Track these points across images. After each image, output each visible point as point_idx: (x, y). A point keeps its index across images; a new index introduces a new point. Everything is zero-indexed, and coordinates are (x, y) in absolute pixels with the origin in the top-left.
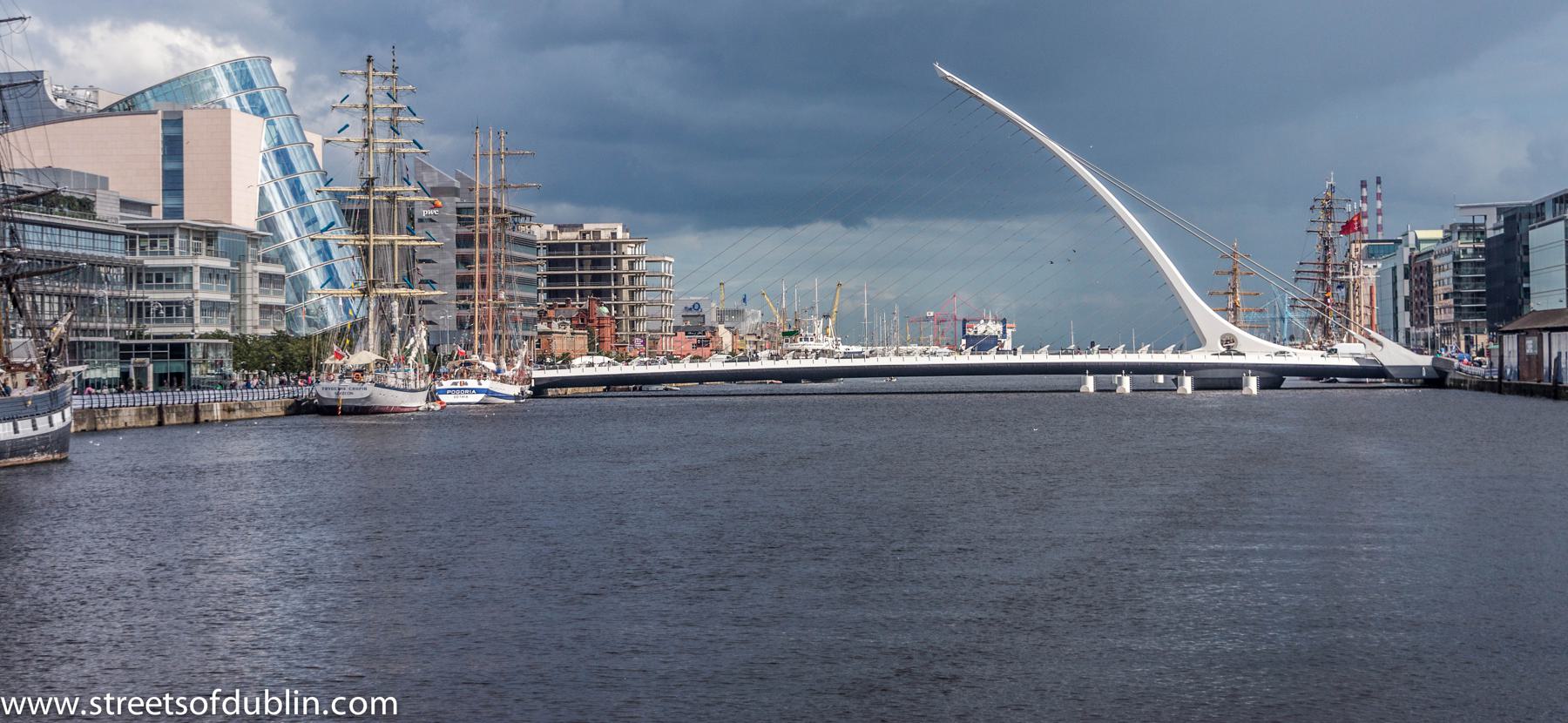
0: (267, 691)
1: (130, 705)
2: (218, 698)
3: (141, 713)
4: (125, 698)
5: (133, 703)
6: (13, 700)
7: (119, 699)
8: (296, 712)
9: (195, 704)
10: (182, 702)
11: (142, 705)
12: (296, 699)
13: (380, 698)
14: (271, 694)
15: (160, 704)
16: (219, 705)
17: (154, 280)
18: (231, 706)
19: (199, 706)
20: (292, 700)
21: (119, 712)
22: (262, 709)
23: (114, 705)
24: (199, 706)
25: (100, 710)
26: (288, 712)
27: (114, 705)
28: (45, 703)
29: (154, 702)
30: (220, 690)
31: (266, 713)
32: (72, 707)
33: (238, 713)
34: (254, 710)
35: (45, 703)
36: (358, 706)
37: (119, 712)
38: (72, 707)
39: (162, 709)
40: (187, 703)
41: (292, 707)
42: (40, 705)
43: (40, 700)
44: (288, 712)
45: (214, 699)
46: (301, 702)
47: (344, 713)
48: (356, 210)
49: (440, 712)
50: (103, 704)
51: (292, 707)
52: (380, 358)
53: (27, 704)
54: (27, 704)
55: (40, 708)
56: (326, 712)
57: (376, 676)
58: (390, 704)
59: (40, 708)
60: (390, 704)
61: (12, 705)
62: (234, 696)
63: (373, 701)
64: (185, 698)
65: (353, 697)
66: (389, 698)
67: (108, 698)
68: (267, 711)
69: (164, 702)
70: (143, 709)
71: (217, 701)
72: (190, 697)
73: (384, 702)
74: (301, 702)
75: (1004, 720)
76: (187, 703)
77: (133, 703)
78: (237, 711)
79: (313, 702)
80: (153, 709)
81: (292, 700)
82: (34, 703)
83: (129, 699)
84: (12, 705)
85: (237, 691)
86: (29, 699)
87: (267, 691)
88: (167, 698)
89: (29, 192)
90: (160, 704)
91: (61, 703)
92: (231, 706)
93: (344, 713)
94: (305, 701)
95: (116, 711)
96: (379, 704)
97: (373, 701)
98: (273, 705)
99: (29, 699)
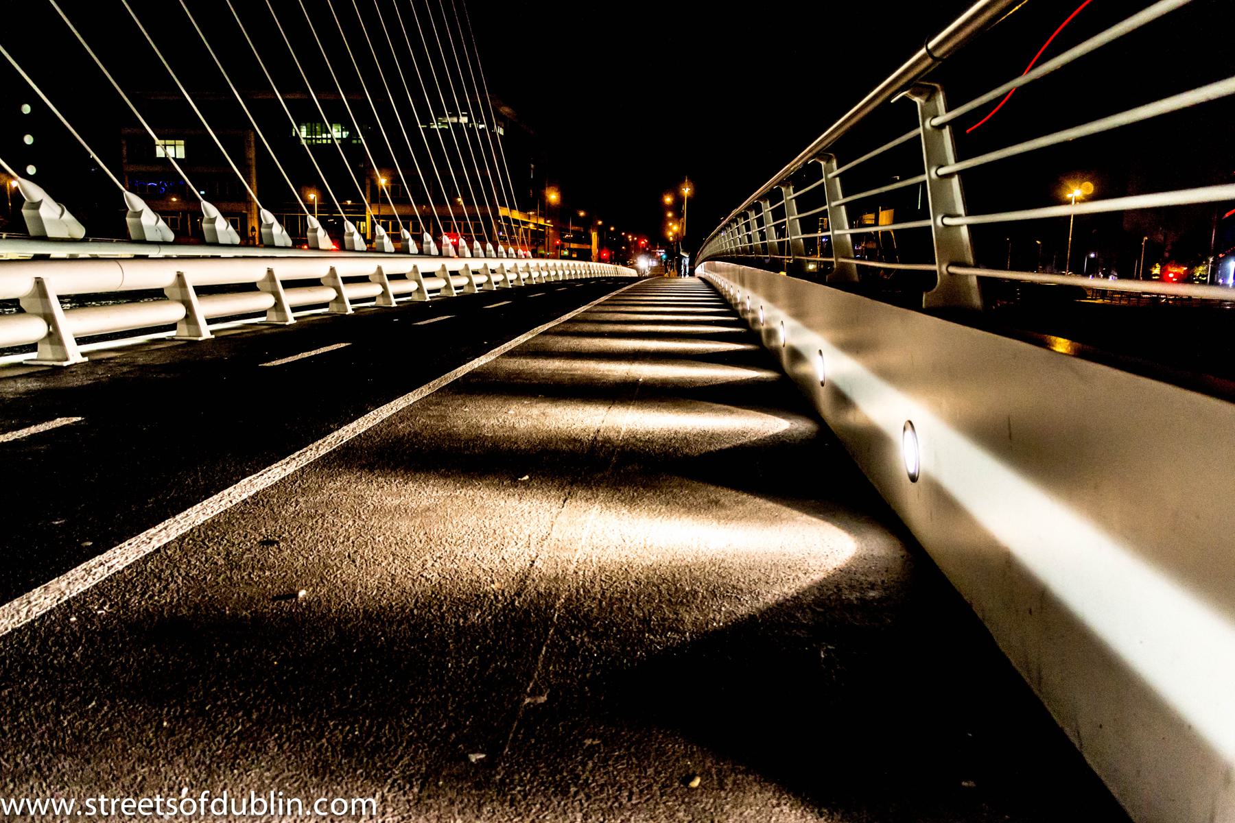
1: (123, 806)
5: (126, 804)
6: (13, 801)
12: (281, 801)
13: (370, 799)
16: (207, 804)
17: (853, 231)
20: (276, 802)
22: (249, 809)
23: (108, 805)
27: (108, 805)
29: (130, 803)
45: (203, 800)
48: (685, 275)
50: (98, 805)
51: (276, 808)
52: (622, 433)
54: (26, 806)
61: (10, 807)
63: (289, 802)
67: (102, 799)
68: (253, 811)
69: (155, 803)
75: (3, 781)
77: (126, 804)
78: (225, 811)
80: (146, 810)
81: (276, 802)
84: (10, 807)
88: (158, 799)
90: (151, 806)
91: (58, 805)
94: (289, 802)
99: (28, 800)
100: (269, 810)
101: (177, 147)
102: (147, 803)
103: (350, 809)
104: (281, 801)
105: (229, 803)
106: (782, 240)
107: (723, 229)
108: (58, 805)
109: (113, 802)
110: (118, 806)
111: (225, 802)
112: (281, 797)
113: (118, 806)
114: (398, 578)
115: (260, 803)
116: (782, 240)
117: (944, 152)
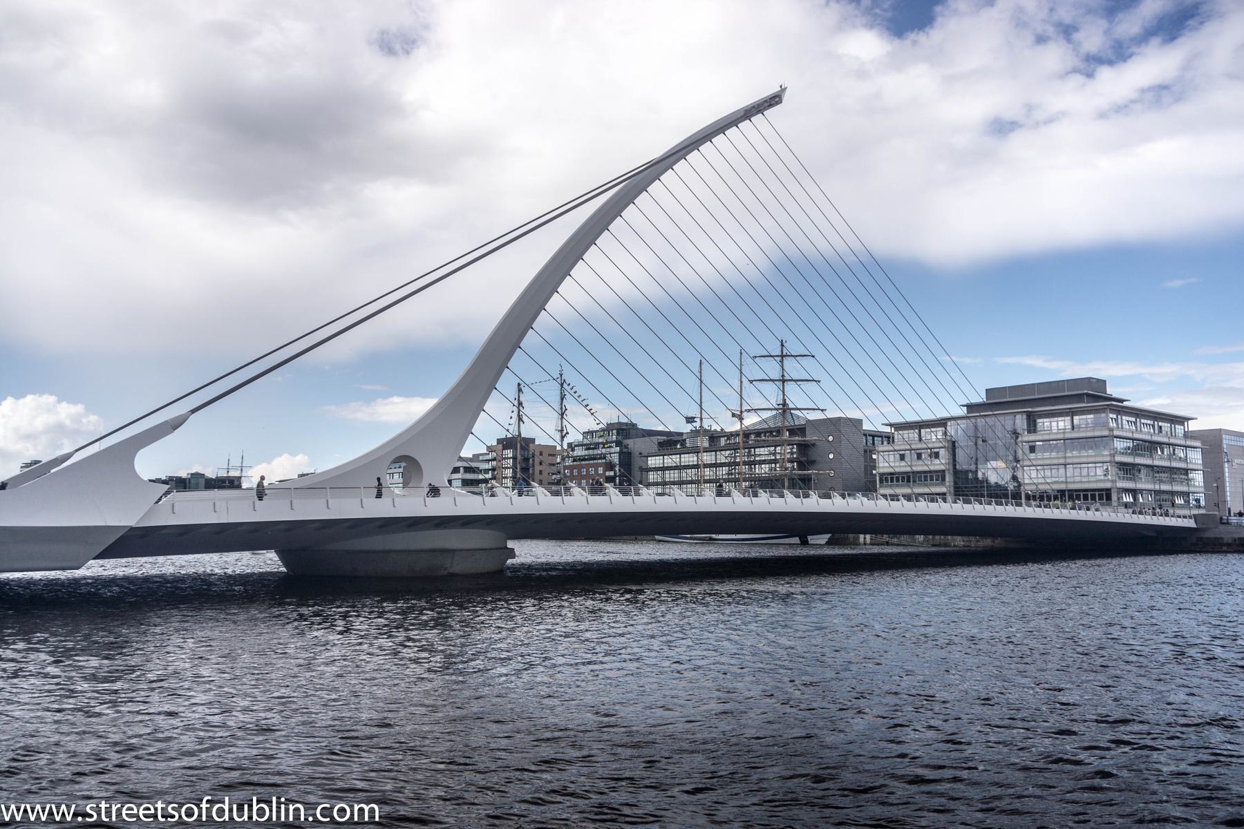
0: (255, 799)
1: (124, 812)
2: (208, 806)
3: (135, 819)
4: (119, 806)
5: (144, 809)
7: (113, 806)
8: (283, 819)
9: (217, 809)
10: (173, 809)
11: (135, 811)
14: (259, 802)
15: (152, 811)
16: (209, 810)
18: (221, 812)
19: (189, 813)
20: (279, 808)
21: (114, 819)
24: (189, 813)
25: (177, 816)
26: (274, 819)
28: (18, 810)
29: (148, 809)
30: (209, 798)
31: (254, 820)
32: (69, 814)
33: (227, 820)
34: (294, 810)
35: (18, 810)
36: (342, 811)
37: (114, 819)
38: (69, 814)
39: (155, 816)
40: (178, 810)
41: (279, 812)
42: (38, 812)
43: (63, 807)
44: (274, 819)
45: (204, 805)
46: (287, 810)
47: (328, 819)
49: (594, 620)
51: (279, 812)
53: (25, 811)
54: (25, 811)
55: (13, 815)
56: (311, 819)
57: (70, 704)
58: (372, 811)
59: (13, 815)
60: (372, 811)
62: (223, 802)
64: (176, 806)
65: (184, 804)
66: (108, 820)
67: (103, 805)
68: (255, 817)
69: (156, 809)
70: (137, 816)
71: (162, 808)
72: (181, 805)
73: (366, 808)
74: (287, 810)
76: (178, 810)
77: (144, 809)
78: (226, 817)
79: (373, 808)
80: (145, 816)
81: (279, 808)
82: (58, 808)
83: (122, 806)
85: (227, 799)
86: (53, 806)
87: (255, 799)
89: (445, 823)
90: (152, 811)
92: (221, 812)
93: (328, 819)
95: (110, 817)
96: (361, 810)
97: (356, 808)
98: (261, 813)
99: (53, 806)
100: (200, 815)
101: (787, 377)
102: (148, 809)
103: (200, 815)
104: (283, 806)
105: (231, 810)
106: (1023, 496)
107: (1016, 496)
108: (33, 810)
109: (114, 809)
110: (119, 811)
111: (226, 808)
112: (283, 803)
113: (119, 811)
114: (789, 688)
115: (262, 809)
116: (1023, 496)
117: (1058, 405)
